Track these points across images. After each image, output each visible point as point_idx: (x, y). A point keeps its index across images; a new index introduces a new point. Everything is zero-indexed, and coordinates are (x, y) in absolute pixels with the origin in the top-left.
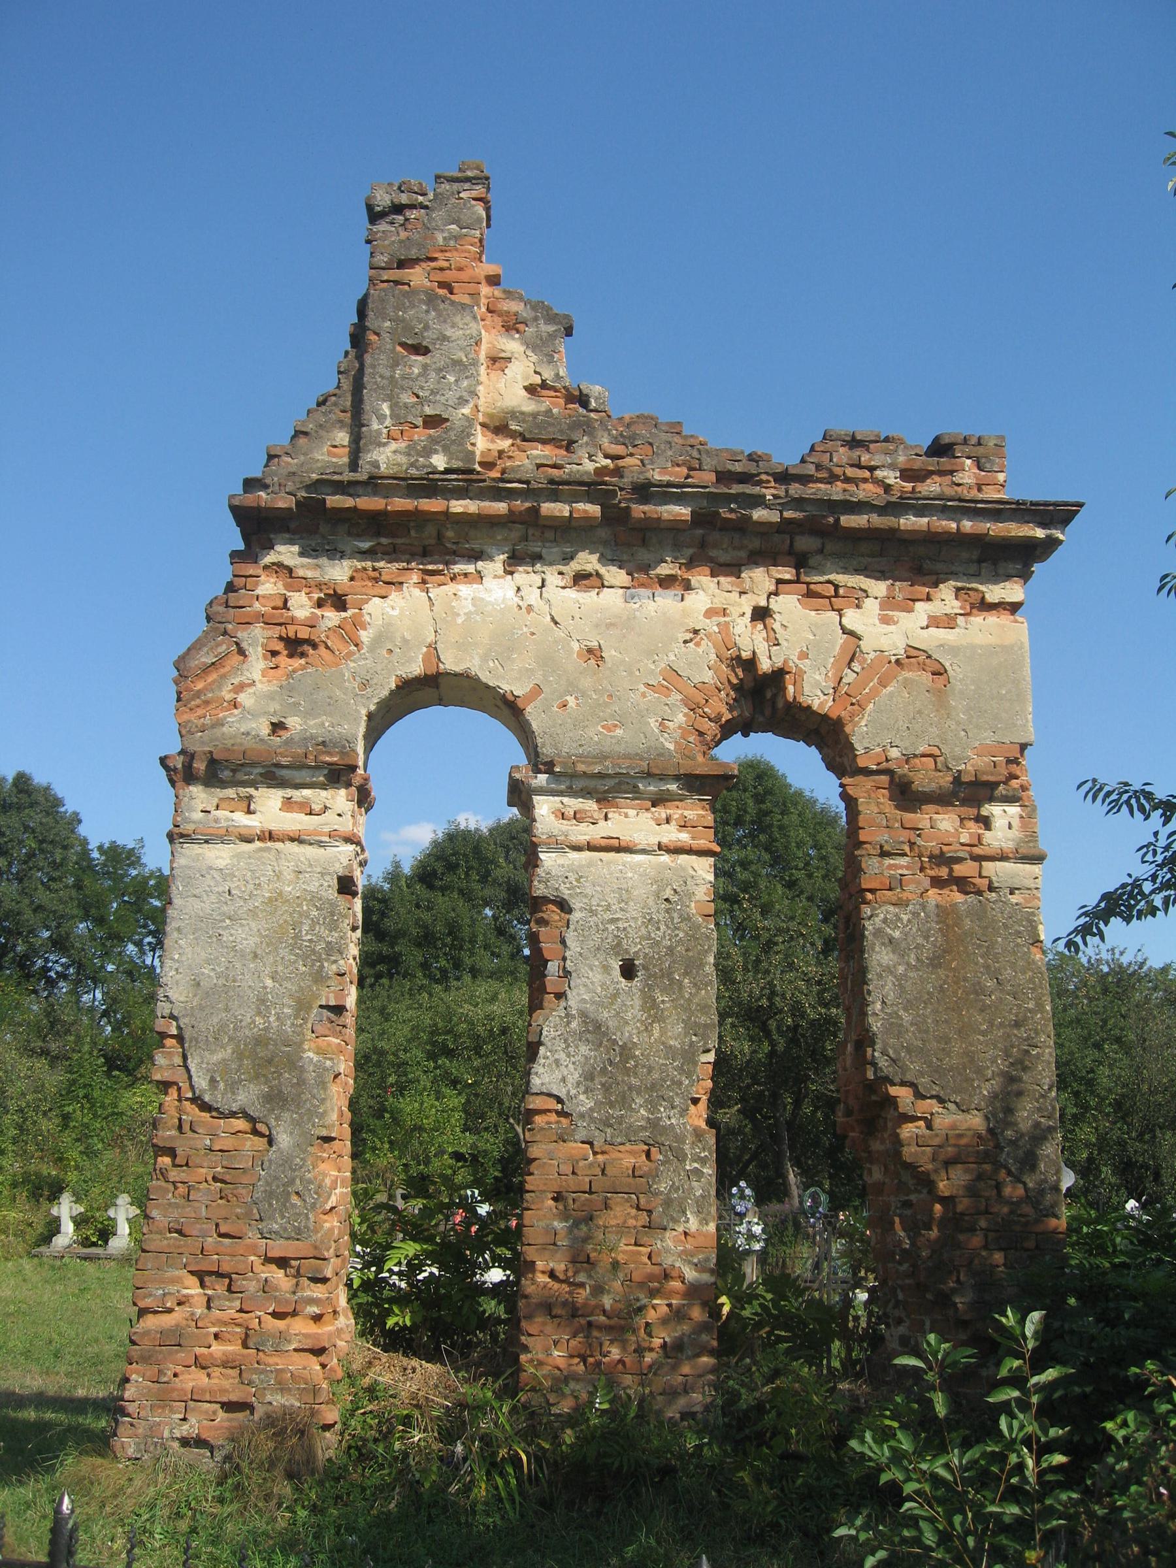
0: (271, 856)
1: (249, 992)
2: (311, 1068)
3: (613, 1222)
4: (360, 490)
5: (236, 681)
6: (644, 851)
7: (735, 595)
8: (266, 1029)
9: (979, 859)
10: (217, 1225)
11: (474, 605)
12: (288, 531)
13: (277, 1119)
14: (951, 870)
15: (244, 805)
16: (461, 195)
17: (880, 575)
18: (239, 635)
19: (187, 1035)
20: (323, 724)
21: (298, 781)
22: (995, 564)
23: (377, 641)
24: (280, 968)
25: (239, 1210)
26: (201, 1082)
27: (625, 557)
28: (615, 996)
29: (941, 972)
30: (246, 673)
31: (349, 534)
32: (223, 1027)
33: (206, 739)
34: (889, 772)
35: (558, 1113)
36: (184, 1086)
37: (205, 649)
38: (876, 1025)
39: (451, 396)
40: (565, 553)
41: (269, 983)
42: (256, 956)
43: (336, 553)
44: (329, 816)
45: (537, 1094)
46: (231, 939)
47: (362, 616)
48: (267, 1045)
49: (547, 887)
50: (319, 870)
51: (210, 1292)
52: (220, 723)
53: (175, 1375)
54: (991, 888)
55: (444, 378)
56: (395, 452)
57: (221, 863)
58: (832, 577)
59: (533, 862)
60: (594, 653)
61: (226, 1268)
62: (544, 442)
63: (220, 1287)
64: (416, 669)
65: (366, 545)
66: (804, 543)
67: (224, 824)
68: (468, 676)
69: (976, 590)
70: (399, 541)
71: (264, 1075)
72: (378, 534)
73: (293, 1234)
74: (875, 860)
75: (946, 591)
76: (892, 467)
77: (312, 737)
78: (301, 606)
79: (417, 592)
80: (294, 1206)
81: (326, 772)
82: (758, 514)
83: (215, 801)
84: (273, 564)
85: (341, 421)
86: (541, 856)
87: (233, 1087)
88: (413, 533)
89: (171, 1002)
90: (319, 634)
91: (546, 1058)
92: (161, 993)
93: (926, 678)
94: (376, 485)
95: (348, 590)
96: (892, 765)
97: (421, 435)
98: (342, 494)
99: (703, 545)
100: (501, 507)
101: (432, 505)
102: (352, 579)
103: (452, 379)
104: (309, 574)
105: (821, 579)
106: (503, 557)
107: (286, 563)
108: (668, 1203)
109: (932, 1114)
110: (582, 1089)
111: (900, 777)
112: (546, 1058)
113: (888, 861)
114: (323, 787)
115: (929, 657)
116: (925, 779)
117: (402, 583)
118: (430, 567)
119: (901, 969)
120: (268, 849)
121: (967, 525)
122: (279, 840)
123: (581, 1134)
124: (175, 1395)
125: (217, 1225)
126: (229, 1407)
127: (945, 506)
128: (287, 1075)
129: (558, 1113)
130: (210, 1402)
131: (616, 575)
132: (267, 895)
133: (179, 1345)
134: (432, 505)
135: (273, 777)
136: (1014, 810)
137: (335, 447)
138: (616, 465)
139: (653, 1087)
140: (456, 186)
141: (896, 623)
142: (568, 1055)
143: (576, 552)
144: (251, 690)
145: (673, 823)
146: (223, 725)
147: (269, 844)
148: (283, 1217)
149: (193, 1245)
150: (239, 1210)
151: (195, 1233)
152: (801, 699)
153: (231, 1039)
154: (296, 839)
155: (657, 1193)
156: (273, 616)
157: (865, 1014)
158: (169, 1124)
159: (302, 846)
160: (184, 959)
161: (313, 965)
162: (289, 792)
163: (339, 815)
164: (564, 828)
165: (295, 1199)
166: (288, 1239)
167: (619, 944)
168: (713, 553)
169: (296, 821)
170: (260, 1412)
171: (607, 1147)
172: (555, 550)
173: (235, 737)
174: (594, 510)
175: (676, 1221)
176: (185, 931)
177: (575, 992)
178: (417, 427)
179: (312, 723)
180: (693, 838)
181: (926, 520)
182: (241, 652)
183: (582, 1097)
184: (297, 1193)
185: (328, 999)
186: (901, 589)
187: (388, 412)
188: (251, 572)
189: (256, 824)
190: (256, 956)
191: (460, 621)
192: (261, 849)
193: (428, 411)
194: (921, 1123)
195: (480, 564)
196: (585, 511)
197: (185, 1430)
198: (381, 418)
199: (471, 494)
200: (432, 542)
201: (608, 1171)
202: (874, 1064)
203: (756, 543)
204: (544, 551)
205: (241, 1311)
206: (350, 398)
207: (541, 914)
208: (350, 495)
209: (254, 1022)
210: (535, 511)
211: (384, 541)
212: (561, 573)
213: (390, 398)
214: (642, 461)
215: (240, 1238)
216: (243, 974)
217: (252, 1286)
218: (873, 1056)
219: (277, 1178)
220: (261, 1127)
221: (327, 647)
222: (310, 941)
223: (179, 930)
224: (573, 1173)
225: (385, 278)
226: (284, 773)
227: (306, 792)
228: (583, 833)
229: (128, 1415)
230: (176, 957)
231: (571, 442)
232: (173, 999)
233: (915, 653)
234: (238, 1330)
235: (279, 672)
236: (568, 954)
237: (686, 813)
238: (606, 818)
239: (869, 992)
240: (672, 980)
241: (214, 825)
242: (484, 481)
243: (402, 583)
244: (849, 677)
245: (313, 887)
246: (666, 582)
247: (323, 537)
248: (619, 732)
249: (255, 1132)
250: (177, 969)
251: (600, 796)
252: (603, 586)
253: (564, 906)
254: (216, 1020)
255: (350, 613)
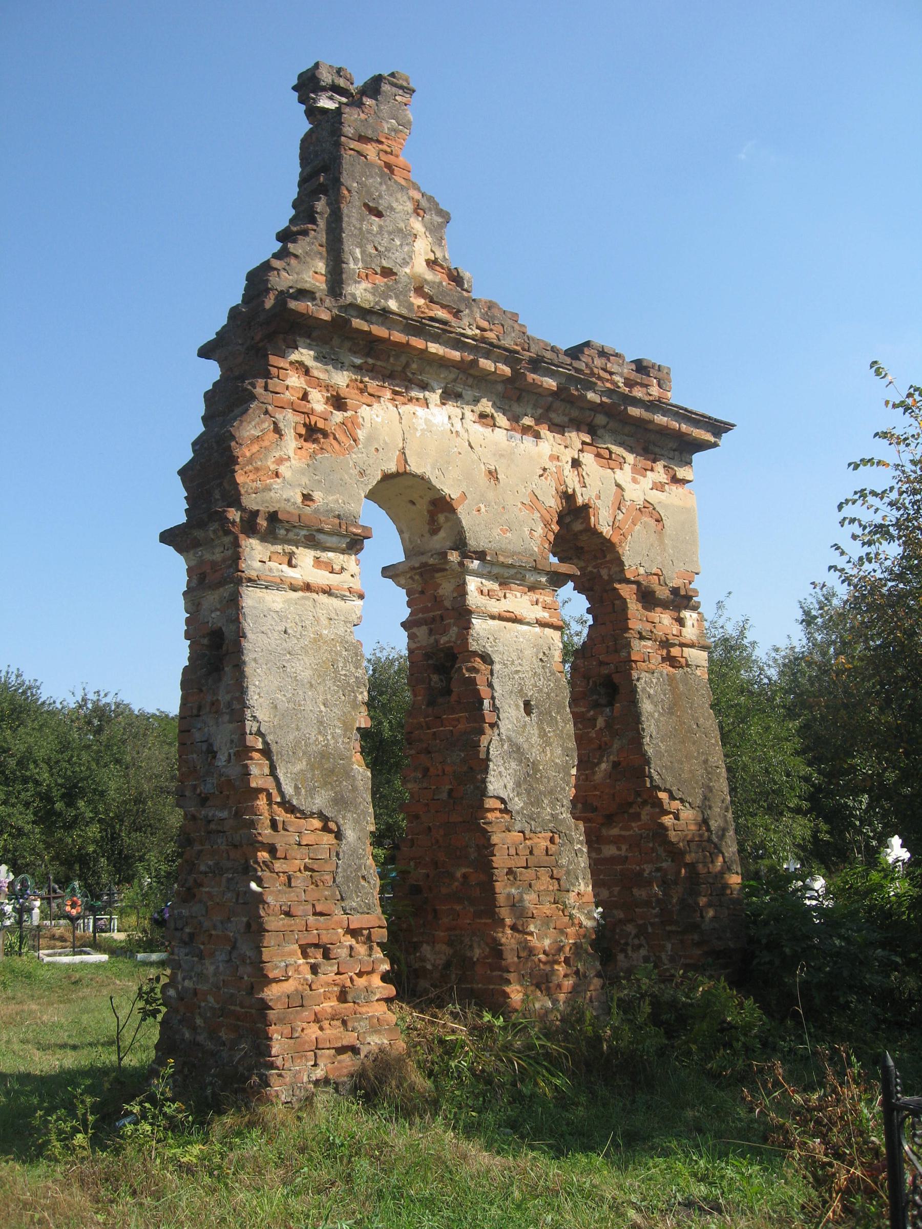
0: (309, 603)
1: (311, 714)
2: (360, 778)
3: (542, 888)
4: (374, 319)
5: (277, 455)
6: (529, 624)
7: (562, 447)
8: (326, 746)
9: (682, 645)
10: (314, 906)
11: (426, 424)
12: (309, 337)
13: (344, 818)
14: (669, 652)
15: (286, 559)
16: (397, 98)
17: (631, 450)
18: (277, 416)
19: (274, 748)
20: (338, 501)
21: (328, 545)
22: (681, 453)
23: (370, 439)
24: (329, 697)
25: (327, 893)
26: (288, 789)
27: (507, 407)
28: (525, 726)
29: (673, 717)
30: (284, 449)
31: (350, 350)
32: (297, 743)
33: (259, 500)
34: (637, 583)
35: (501, 811)
36: (274, 792)
37: (253, 423)
38: (650, 751)
39: (398, 256)
40: (475, 397)
41: (323, 708)
42: (311, 685)
43: (339, 365)
44: (345, 576)
45: (491, 797)
46: (293, 670)
47: (357, 417)
48: (328, 758)
49: (478, 644)
50: (343, 618)
51: (312, 961)
52: (268, 489)
53: (303, 1030)
54: (688, 665)
55: (393, 240)
56: (365, 290)
57: (278, 606)
58: (609, 446)
59: (468, 626)
60: (493, 474)
61: (325, 939)
62: (443, 306)
63: (317, 957)
64: (392, 467)
65: (358, 361)
66: (601, 419)
67: (276, 574)
68: (423, 478)
69: (673, 469)
70: (379, 363)
71: (330, 783)
72: (368, 355)
73: (365, 910)
74: (637, 641)
75: (659, 466)
76: (621, 375)
77: (332, 510)
78: (318, 402)
79: (390, 406)
80: (363, 886)
81: (348, 540)
82: (590, 395)
83: (269, 554)
84: (297, 362)
85: (320, 254)
86: (474, 621)
87: (311, 792)
88: (392, 360)
89: (258, 721)
90: (331, 427)
91: (494, 771)
92: (248, 713)
93: (652, 522)
94: (387, 318)
95: (347, 395)
96: (640, 579)
97: (380, 281)
98: (362, 319)
99: (549, 409)
100: (456, 355)
101: (418, 343)
102: (348, 386)
103: (398, 243)
104: (322, 376)
105: (604, 446)
106: (440, 391)
107: (306, 363)
108: (568, 873)
109: (678, 810)
110: (515, 793)
111: (646, 587)
112: (494, 771)
113: (643, 643)
114: (343, 552)
115: (654, 509)
116: (663, 593)
117: (379, 397)
118: (397, 389)
119: (656, 715)
120: (307, 598)
121: (684, 427)
122: (314, 591)
123: (518, 826)
124: (307, 1047)
125: (314, 906)
126: (341, 1050)
127: (677, 412)
128: (345, 783)
129: (501, 811)
130: (328, 1049)
131: (502, 420)
132: (312, 636)
133: (302, 1006)
134: (418, 343)
135: (312, 542)
136: (695, 615)
137: (316, 273)
138: (482, 335)
139: (551, 792)
140: (394, 89)
141: (639, 483)
142: (506, 768)
143: (481, 397)
144: (287, 464)
145: (540, 604)
146: (270, 490)
147: (308, 594)
148: (358, 896)
149: (298, 923)
150: (327, 893)
151: (299, 913)
152: (598, 527)
153: (304, 753)
154: (328, 592)
155: (562, 867)
156: (299, 406)
157: (642, 744)
158: (265, 825)
159: (331, 598)
160: (263, 685)
161: (350, 695)
162: (318, 553)
163: (352, 576)
164: (484, 602)
165: (363, 883)
166: (362, 913)
167: (522, 689)
168: (553, 415)
169: (321, 578)
170: (364, 1051)
171: (532, 835)
172: (469, 392)
173: (278, 501)
174: (506, 370)
175: (574, 885)
176: (260, 661)
177: (503, 722)
178: (376, 274)
179: (331, 498)
180: (550, 617)
181: (666, 419)
182: (277, 430)
183: (516, 799)
184: (363, 877)
185: (360, 723)
186: (643, 462)
187: (359, 256)
188: (281, 365)
189: (298, 576)
190: (311, 685)
191: (418, 434)
192: (303, 598)
193: (385, 263)
194: (671, 816)
195: (427, 393)
196: (503, 370)
197: (319, 1073)
198: (355, 260)
199: (441, 341)
200: (400, 369)
201: (535, 852)
202: (651, 777)
203: (575, 413)
204: (464, 392)
205: (338, 973)
206: (325, 236)
207: (470, 664)
208: (366, 321)
209: (317, 739)
210: (475, 363)
211: (370, 361)
212: (472, 411)
213: (361, 246)
214: (497, 336)
215: (329, 915)
216: (305, 700)
217: (343, 953)
218: (650, 772)
219: (350, 866)
220: (332, 825)
221: (335, 438)
222: (345, 675)
223: (255, 660)
224: (517, 854)
225: (352, 147)
226: (321, 537)
227: (331, 555)
228: (495, 607)
229: (277, 1068)
230: (257, 683)
231: (459, 311)
232: (260, 719)
233: (647, 505)
234: (336, 989)
235: (303, 451)
236: (496, 694)
237: (546, 598)
238: (505, 597)
239: (643, 730)
240: (551, 716)
241: (268, 573)
242: (452, 332)
243: (379, 397)
244: (620, 516)
245: (341, 632)
246: (526, 430)
247: (332, 348)
248: (508, 534)
249: (326, 829)
250: (259, 694)
251: (502, 580)
252: (495, 425)
253: (487, 659)
254: (292, 737)
255: (349, 414)
